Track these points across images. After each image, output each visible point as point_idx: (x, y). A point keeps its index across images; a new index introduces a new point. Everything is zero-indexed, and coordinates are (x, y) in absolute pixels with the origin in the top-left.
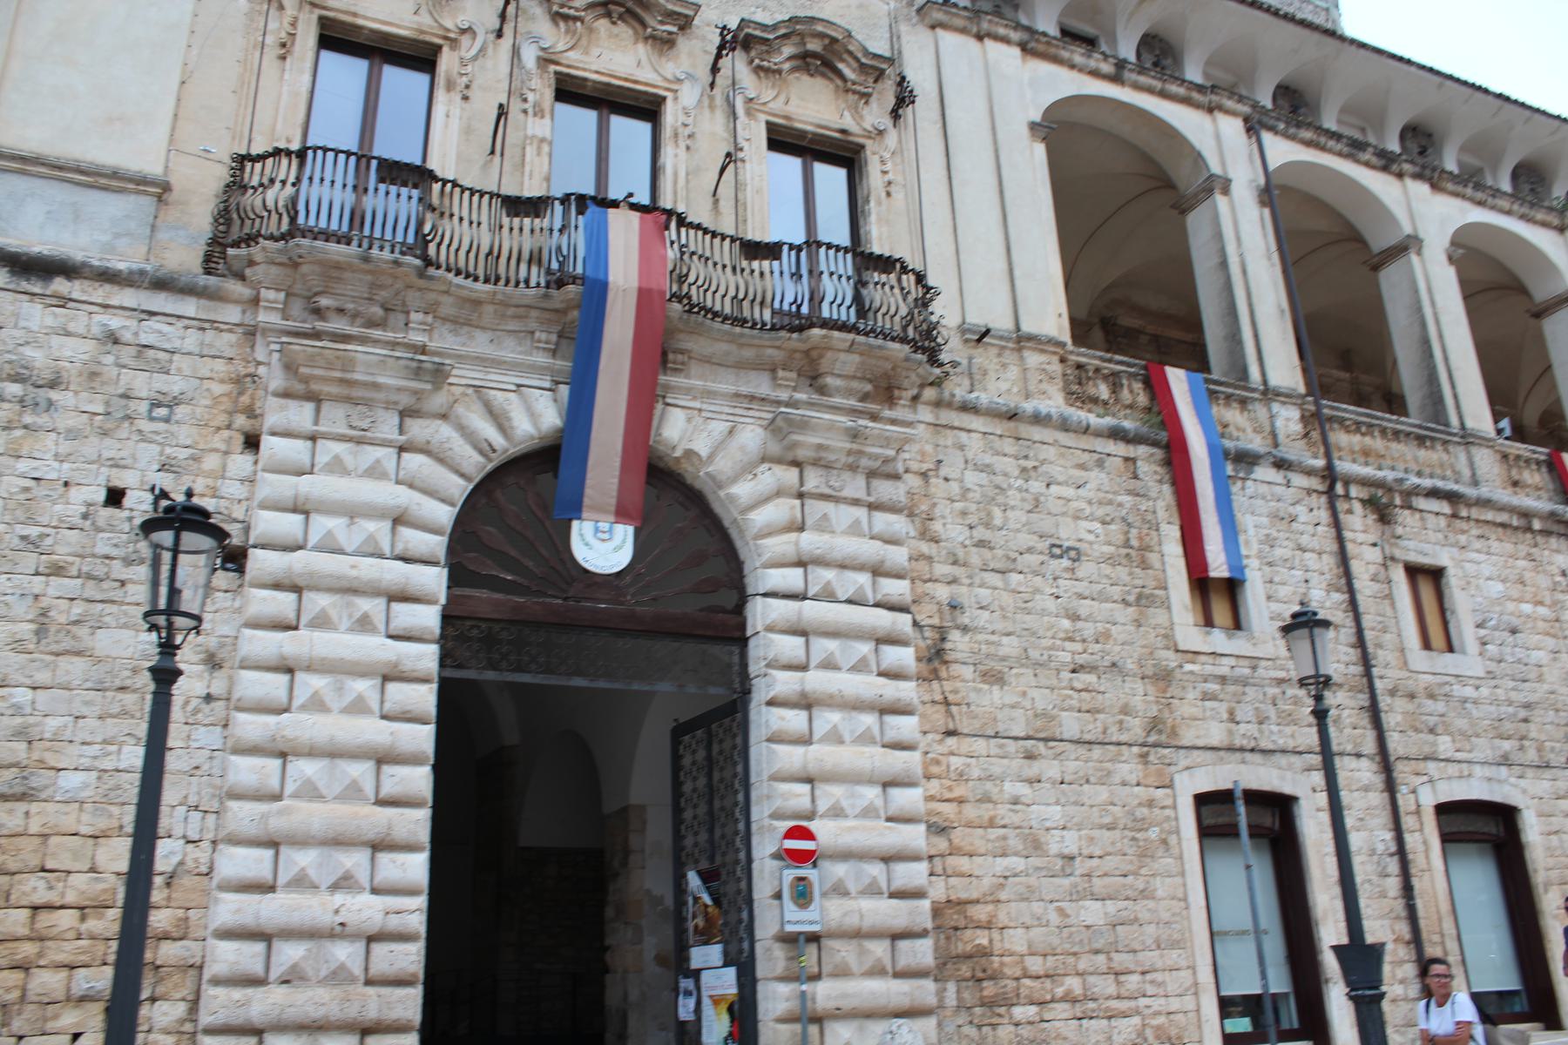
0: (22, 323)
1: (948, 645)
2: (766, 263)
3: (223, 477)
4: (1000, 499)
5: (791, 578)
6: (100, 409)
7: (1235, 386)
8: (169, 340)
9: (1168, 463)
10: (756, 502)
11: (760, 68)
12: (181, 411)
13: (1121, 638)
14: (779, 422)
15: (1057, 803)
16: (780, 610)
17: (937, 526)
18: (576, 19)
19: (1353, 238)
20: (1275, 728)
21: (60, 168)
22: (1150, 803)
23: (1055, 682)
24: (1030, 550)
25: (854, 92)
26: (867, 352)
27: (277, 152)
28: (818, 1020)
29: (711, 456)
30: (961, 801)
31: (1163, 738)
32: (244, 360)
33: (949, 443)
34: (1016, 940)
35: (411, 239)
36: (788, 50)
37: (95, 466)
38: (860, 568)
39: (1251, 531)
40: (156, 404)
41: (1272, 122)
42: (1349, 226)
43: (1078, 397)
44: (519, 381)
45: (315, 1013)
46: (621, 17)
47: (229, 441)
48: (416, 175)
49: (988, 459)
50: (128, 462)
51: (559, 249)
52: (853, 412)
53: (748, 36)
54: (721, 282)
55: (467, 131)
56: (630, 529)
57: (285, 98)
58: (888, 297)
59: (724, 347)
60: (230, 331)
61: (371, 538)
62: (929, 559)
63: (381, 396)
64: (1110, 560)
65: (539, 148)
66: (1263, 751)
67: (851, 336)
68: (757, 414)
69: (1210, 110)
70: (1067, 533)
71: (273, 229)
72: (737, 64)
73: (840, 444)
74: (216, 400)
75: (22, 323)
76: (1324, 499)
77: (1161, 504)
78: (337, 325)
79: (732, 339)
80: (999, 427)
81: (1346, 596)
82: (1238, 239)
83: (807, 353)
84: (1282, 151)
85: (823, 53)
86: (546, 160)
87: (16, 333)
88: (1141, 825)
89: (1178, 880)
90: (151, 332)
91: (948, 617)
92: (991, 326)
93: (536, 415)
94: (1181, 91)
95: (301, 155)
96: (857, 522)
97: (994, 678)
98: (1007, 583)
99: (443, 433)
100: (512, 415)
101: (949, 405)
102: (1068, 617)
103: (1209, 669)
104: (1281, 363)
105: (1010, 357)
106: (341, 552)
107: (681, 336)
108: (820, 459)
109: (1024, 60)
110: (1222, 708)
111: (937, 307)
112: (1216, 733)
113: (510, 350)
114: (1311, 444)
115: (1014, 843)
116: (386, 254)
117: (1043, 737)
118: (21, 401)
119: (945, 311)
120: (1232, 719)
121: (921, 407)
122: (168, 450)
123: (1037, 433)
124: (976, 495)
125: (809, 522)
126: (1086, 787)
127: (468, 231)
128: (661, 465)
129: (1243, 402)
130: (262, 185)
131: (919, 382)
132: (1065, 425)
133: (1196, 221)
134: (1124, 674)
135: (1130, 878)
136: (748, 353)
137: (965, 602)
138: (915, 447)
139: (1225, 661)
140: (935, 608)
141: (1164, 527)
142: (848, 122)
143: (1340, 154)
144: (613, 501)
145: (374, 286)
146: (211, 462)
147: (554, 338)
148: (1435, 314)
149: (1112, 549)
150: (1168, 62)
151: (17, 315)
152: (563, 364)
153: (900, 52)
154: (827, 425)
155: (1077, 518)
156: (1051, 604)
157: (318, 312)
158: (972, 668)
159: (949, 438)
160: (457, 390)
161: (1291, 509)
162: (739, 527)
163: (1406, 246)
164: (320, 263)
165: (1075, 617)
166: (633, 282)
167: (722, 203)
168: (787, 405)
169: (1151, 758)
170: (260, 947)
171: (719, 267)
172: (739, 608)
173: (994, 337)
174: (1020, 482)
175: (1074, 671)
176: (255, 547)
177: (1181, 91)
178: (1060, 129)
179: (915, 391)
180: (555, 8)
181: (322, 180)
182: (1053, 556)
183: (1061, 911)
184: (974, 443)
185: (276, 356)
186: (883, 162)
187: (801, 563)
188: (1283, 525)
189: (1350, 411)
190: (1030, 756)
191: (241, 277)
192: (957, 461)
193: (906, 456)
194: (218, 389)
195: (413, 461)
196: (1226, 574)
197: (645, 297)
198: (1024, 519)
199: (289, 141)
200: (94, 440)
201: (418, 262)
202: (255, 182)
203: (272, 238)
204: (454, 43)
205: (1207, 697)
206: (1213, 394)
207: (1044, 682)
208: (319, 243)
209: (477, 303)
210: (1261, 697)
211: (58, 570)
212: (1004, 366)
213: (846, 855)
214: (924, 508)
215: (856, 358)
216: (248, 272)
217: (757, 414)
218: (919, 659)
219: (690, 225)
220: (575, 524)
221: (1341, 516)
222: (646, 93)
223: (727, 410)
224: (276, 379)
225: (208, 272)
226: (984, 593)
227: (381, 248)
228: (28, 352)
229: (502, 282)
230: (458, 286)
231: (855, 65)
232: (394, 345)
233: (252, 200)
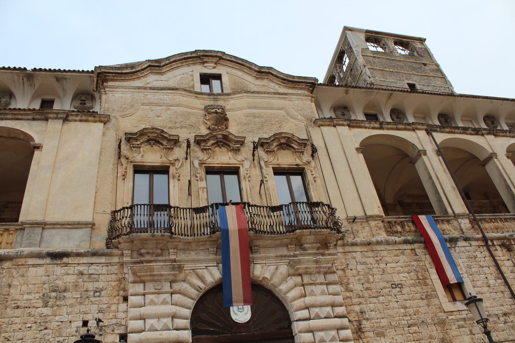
0: (55, 273)
1: (362, 326)
2: (278, 212)
3: (118, 312)
4: (371, 272)
5: (304, 313)
6: (79, 297)
7: (445, 216)
8: (98, 271)
9: (426, 248)
10: (289, 290)
11: (267, 151)
12: (103, 293)
13: (423, 312)
14: (291, 263)
16: (302, 325)
17: (351, 286)
18: (208, 149)
19: (473, 158)
21: (64, 225)
24: (384, 288)
25: (298, 152)
26: (316, 234)
27: (124, 208)
29: (271, 278)
32: (121, 273)
33: (350, 257)
35: (166, 226)
36: (275, 144)
37: (78, 315)
38: (327, 305)
39: (461, 265)
40: (95, 292)
41: (435, 129)
42: (471, 154)
43: (391, 232)
44: (206, 265)
46: (222, 146)
47: (118, 300)
48: (167, 207)
49: (364, 260)
50: (89, 311)
51: (212, 222)
52: (315, 254)
53: (262, 142)
54: (265, 221)
55: (181, 190)
56: (249, 306)
57: (125, 190)
58: (321, 214)
59: (270, 241)
60: (116, 265)
61: (165, 325)
63: (163, 278)
64: (413, 285)
65: (203, 191)
67: (310, 230)
68: (284, 261)
69: (414, 130)
70: (396, 279)
71: (125, 232)
72: (260, 151)
73: (313, 266)
74: (113, 287)
75: (55, 273)
76: (485, 248)
77: (427, 262)
78: (148, 257)
79: (272, 239)
80: (365, 249)
81: (503, 280)
82: (433, 168)
83: (297, 238)
84: (440, 137)
85: (286, 142)
86: (206, 194)
87: (53, 277)
90: (93, 269)
91: (360, 316)
92: (356, 216)
93: (213, 275)
94: (403, 127)
95: (131, 207)
96: (323, 290)
98: (379, 300)
99: (184, 286)
100: (205, 276)
101: (347, 245)
102: (403, 308)
103: (458, 317)
104: (458, 205)
105: (365, 225)
106: (157, 330)
107: (255, 241)
108: (307, 272)
109: (350, 130)
110: (467, 330)
111: (337, 214)
113: (202, 256)
114: (475, 230)
116: (159, 233)
118: (56, 297)
119: (340, 215)
120: (472, 333)
121: (338, 248)
122: (100, 306)
123: (379, 248)
124: (362, 273)
125: (307, 294)
127: (183, 221)
128: (256, 283)
129: (448, 221)
130: (120, 219)
131: (335, 240)
132: (388, 243)
133: (418, 165)
134: (427, 325)
136: (278, 242)
138: (339, 261)
139: (463, 312)
140: (355, 314)
141: (430, 270)
142: (298, 162)
143: (461, 133)
144: (242, 298)
145: (157, 244)
146: (114, 307)
147: (215, 249)
148: (508, 176)
150: (401, 116)
151: (53, 271)
152: (219, 257)
153: (310, 136)
154: (307, 261)
155: (398, 273)
156: (396, 305)
157: (141, 255)
158: (372, 333)
159: (349, 256)
160: (187, 272)
161: (474, 254)
162: (284, 299)
163: (492, 156)
164: (140, 240)
165: (405, 308)
166: (236, 228)
167: (262, 195)
168: (293, 256)
171: (264, 217)
172: (290, 327)
173: (358, 219)
174: (376, 265)
175: (409, 327)
176: (129, 333)
177: (403, 127)
178: (366, 148)
179: (335, 243)
180: (202, 147)
181: (137, 214)
182: (393, 288)
184: (358, 256)
185: (130, 270)
186: (311, 172)
187: (307, 308)
188: (473, 260)
189: (487, 216)
191: (118, 248)
192: (354, 262)
193: (336, 264)
194: (114, 284)
195: (176, 297)
196: (456, 282)
197: (241, 231)
198: (380, 278)
199: (128, 203)
200: (78, 306)
201: (169, 234)
202: (118, 219)
203: (125, 235)
204: (173, 164)
205: (459, 327)
206: (437, 221)
207: (399, 333)
208: (138, 234)
209: (189, 243)
212: (363, 228)
214: (345, 281)
215: (313, 236)
216: (119, 246)
217: (284, 261)
218: (353, 333)
219: (252, 206)
220: (231, 308)
221: (493, 252)
222: (234, 167)
223: (274, 262)
224: (130, 278)
225: (108, 248)
226: (371, 306)
227: (157, 232)
229: (196, 235)
230: (183, 239)
231: (297, 144)
232: (165, 261)
233: (118, 224)
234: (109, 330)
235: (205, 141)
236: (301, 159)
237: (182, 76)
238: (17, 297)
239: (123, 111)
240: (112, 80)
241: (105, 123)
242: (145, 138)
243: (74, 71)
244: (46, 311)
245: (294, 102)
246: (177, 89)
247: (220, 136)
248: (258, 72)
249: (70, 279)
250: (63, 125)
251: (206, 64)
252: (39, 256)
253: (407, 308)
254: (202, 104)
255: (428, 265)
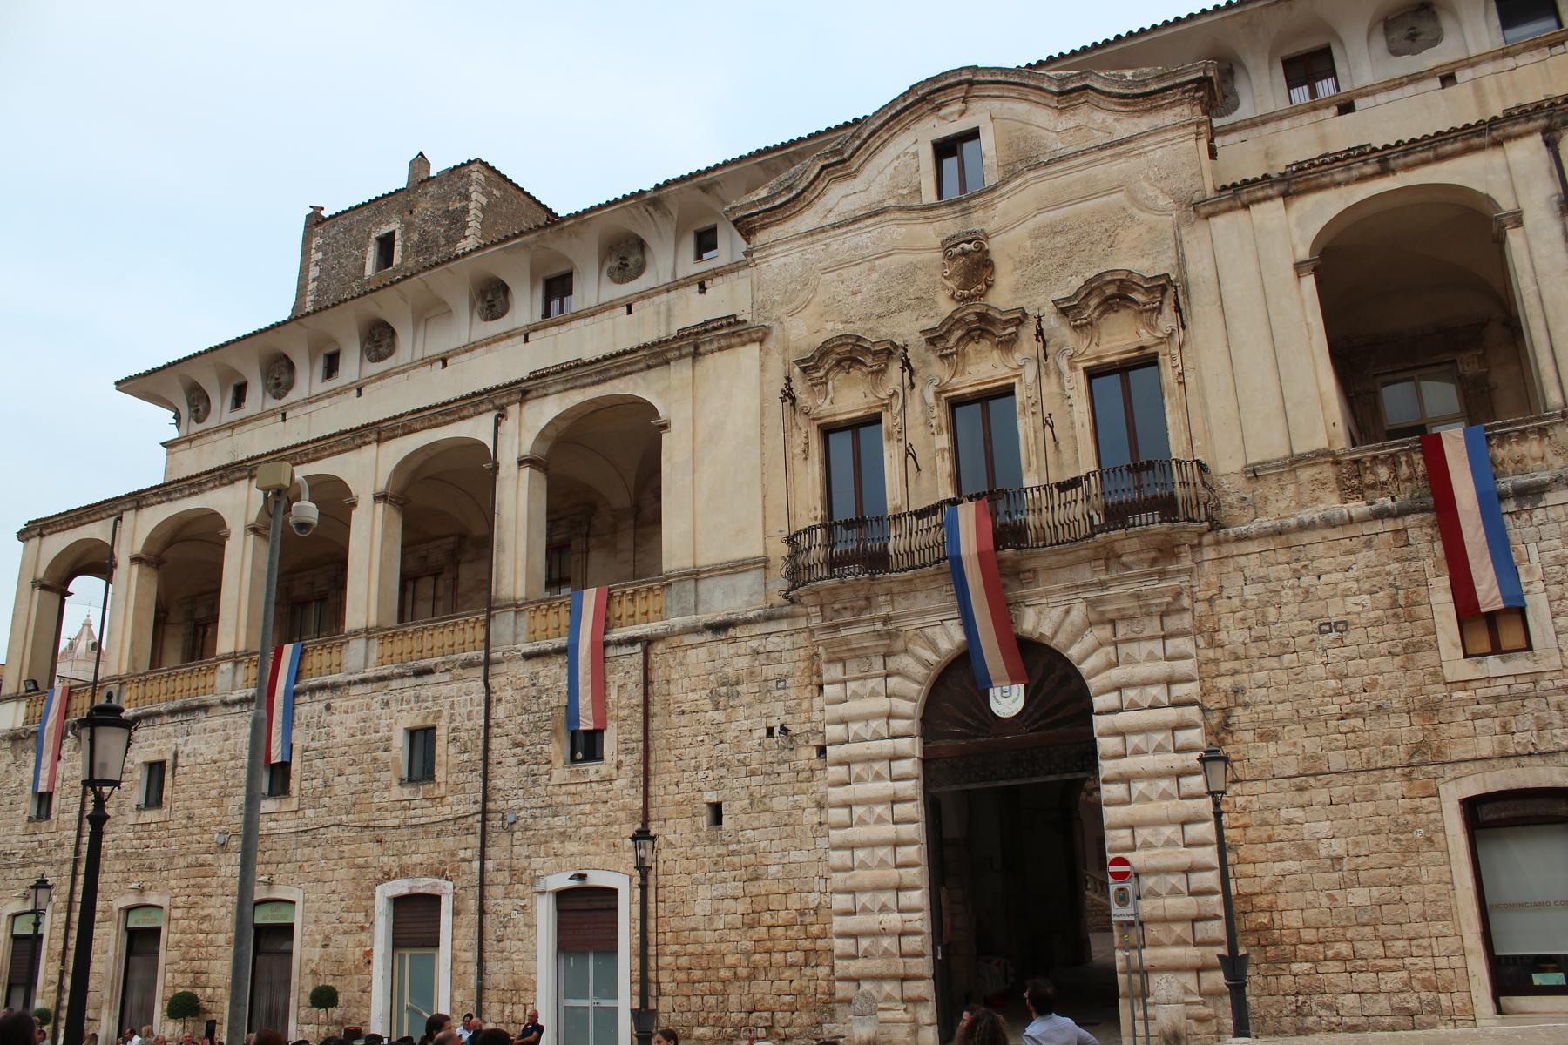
4: (1275, 600)
5: (1111, 700)
10: (1088, 655)
12: (789, 681)
13: (1387, 685)
15: (1327, 819)
17: (1222, 636)
20: (1558, 732)
22: (1415, 811)
23: (1323, 730)
24: (1301, 633)
28: (1146, 972)
30: (1245, 827)
31: (1429, 758)
34: (1293, 919)
36: (1093, 302)
38: (1156, 683)
39: (1535, 557)
43: (1348, 491)
45: (876, 971)
46: (980, 336)
62: (1216, 661)
66: (1541, 754)
70: (1335, 612)
78: (848, 617)
79: (1056, 553)
85: (1115, 294)
88: (1406, 828)
89: (1446, 868)
90: (772, 643)
93: (950, 638)
97: (1268, 736)
98: (1281, 663)
102: (1336, 678)
103: (1481, 692)
105: (1286, 478)
112: (1486, 746)
115: (1289, 850)
117: (1314, 771)
123: (1306, 538)
126: (1352, 805)
129: (1542, 432)
135: (1395, 869)
136: (1071, 557)
137: (1246, 685)
139: (1500, 682)
141: (1432, 581)
146: (805, 704)
149: (1380, 613)
154: (1120, 593)
156: (1320, 671)
169: (1415, 775)
170: (852, 941)
177: (1458, 145)
182: (1321, 632)
183: (1331, 897)
184: (1252, 565)
190: (1301, 789)
195: (893, 682)
205: (1475, 717)
207: (1312, 731)
209: (910, 581)
210: (1544, 706)
211: (753, 773)
212: (1282, 488)
213: (1156, 872)
226: (1261, 676)
228: (726, 670)
234: (801, 741)
235: (941, 337)
236: (1152, 327)
237: (896, 163)
238: (681, 697)
239: (791, 301)
240: (763, 227)
241: (761, 341)
242: (831, 360)
243: (726, 164)
244: (718, 716)
245: (1151, 155)
246: (884, 211)
247: (972, 317)
248: (1060, 94)
249: (743, 663)
250: (693, 367)
251: (943, 112)
252: (695, 630)
253: (1346, 676)
254: (939, 234)
255: (1429, 570)
